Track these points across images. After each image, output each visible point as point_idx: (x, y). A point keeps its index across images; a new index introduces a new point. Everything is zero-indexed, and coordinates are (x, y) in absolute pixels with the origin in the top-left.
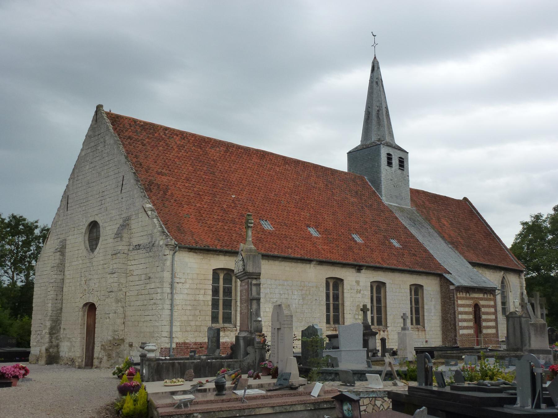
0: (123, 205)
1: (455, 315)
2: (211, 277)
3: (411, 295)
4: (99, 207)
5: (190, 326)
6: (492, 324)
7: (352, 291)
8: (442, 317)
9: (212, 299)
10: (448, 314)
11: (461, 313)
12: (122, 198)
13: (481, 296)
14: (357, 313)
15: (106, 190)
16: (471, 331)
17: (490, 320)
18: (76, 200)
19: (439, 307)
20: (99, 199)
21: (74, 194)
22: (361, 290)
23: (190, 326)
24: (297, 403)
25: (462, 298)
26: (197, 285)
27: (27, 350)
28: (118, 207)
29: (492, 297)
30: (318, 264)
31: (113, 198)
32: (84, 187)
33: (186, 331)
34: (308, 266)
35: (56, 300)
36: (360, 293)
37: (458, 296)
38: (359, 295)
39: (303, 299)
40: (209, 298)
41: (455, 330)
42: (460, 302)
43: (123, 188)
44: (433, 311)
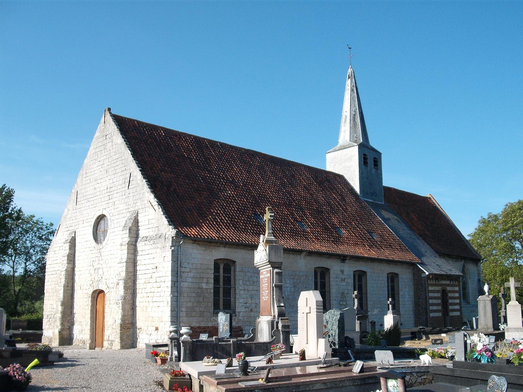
0: (131, 200)
1: (426, 300)
2: (212, 267)
3: (388, 282)
4: (107, 202)
5: (195, 311)
6: (457, 307)
7: (337, 279)
8: (415, 302)
9: (214, 287)
10: (420, 299)
11: (432, 298)
12: (129, 194)
13: (448, 282)
14: (342, 299)
15: (114, 186)
16: (439, 314)
17: (456, 304)
18: (85, 195)
19: (412, 293)
20: (107, 194)
21: (83, 190)
22: (345, 279)
23: (195, 311)
24: (346, 379)
25: (432, 285)
26: (200, 274)
27: (39, 332)
28: (126, 201)
29: (457, 283)
30: (308, 255)
31: (120, 193)
32: (93, 184)
33: (191, 316)
34: (299, 257)
35: (68, 287)
36: (344, 281)
37: (429, 283)
38: (344, 283)
39: (295, 287)
40: (211, 286)
41: (426, 313)
42: (430, 288)
43: (130, 185)
44: (407, 296)
